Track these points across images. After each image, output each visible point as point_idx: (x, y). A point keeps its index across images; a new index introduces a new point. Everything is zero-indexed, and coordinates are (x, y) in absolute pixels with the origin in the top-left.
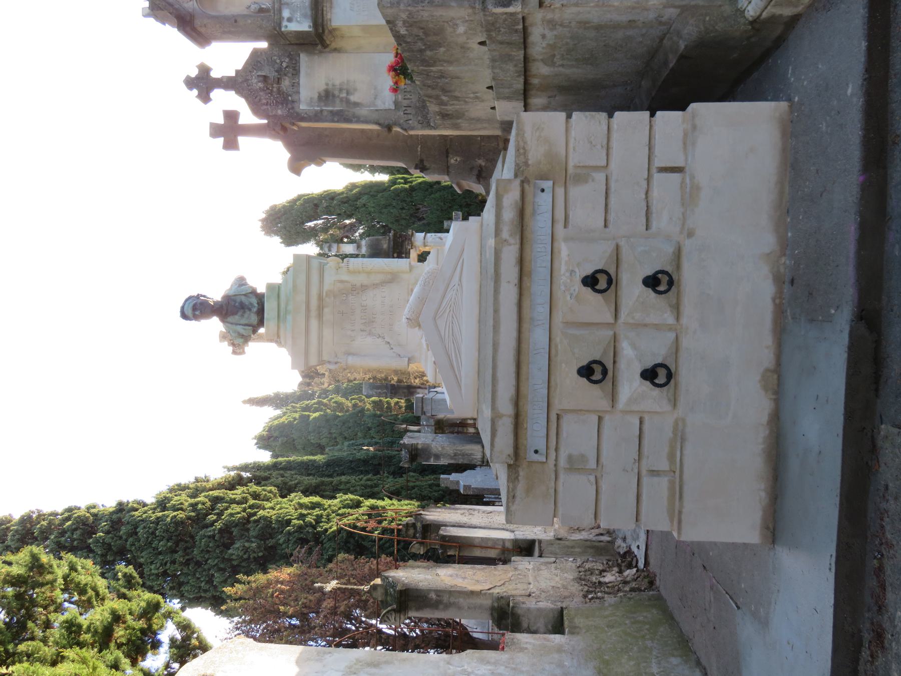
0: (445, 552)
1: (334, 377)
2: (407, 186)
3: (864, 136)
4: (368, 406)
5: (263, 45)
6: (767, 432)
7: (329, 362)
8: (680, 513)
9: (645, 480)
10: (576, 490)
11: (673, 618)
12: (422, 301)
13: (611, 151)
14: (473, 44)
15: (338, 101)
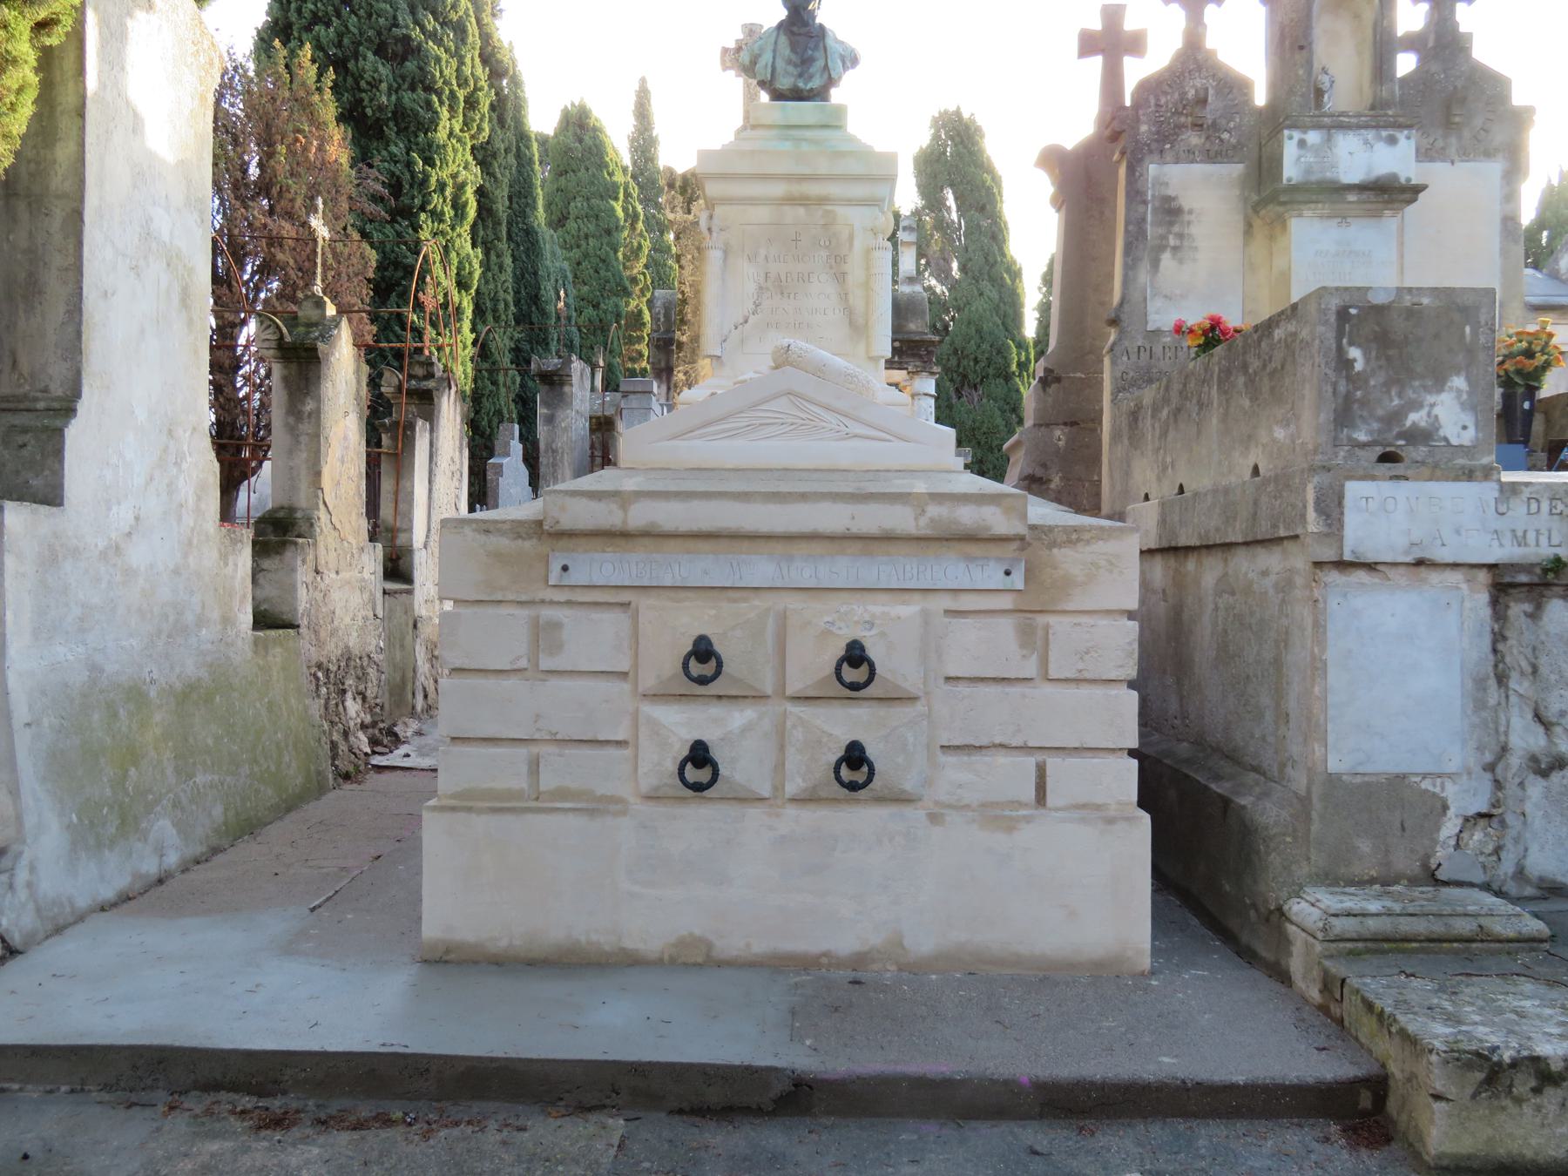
0: (387, 430)
1: (685, 229)
2: (1014, 367)
3: (1092, 1083)
4: (633, 304)
5: (1260, 98)
6: (607, 948)
7: (711, 217)
8: (469, 810)
9: (522, 752)
10: (502, 636)
11: (289, 810)
12: (819, 371)
13: (1073, 685)
14: (1256, 456)
15: (1161, 231)
